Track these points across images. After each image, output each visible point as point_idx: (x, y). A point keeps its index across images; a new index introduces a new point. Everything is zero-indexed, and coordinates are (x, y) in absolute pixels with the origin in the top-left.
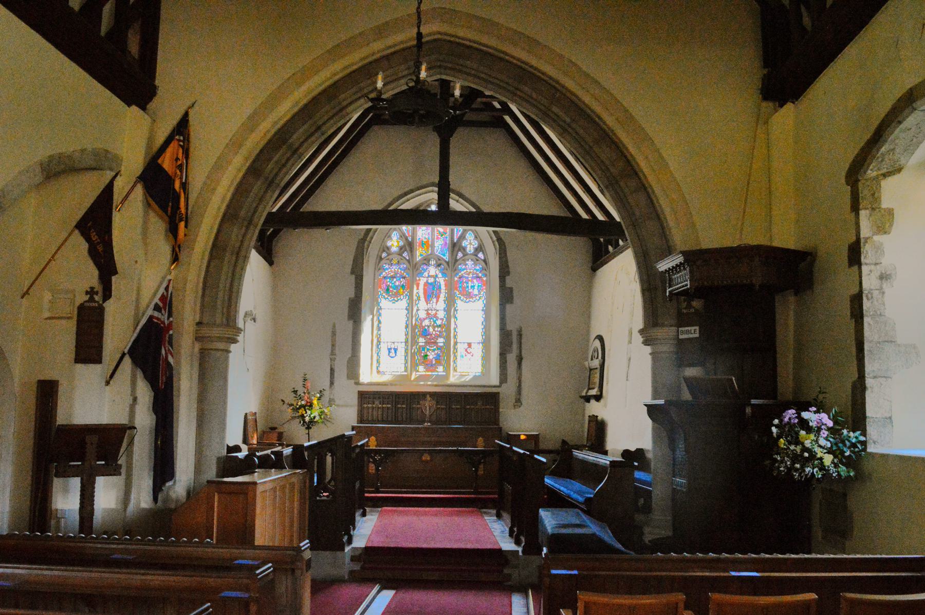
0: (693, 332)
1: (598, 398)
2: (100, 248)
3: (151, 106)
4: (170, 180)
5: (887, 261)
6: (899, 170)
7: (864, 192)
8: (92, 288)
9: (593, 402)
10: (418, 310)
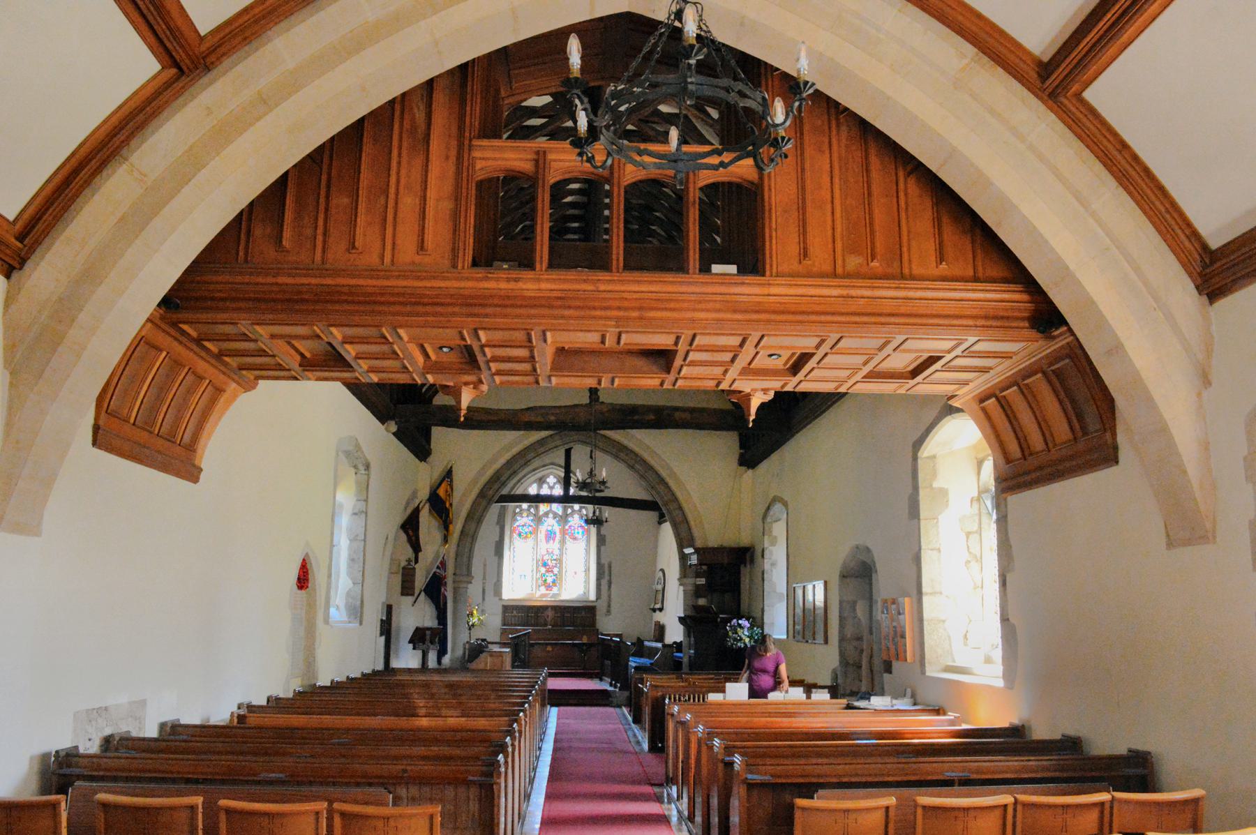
0: (702, 581)
1: (661, 610)
2: (413, 538)
3: (430, 459)
4: (443, 502)
9: (658, 612)
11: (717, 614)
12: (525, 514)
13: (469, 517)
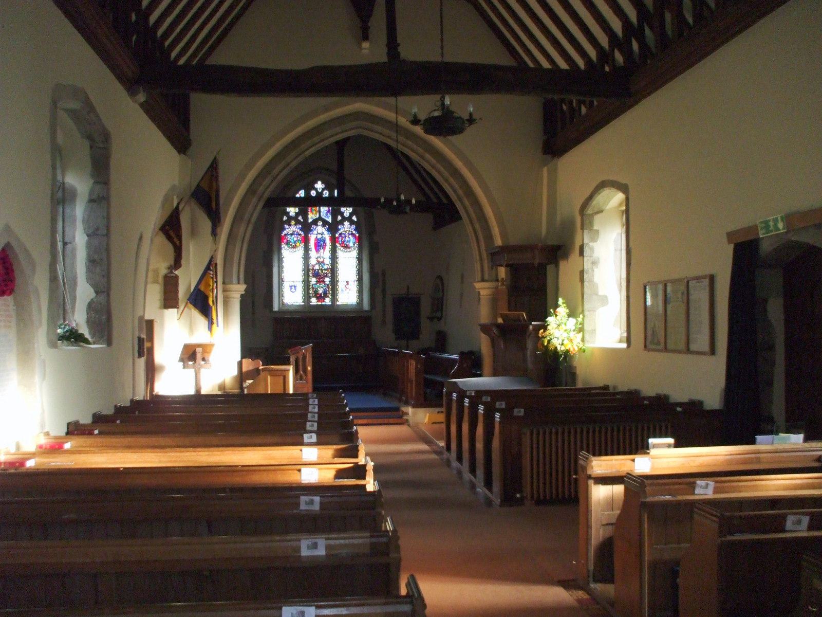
5: (596, 255)
7: (587, 221)
12: (293, 223)
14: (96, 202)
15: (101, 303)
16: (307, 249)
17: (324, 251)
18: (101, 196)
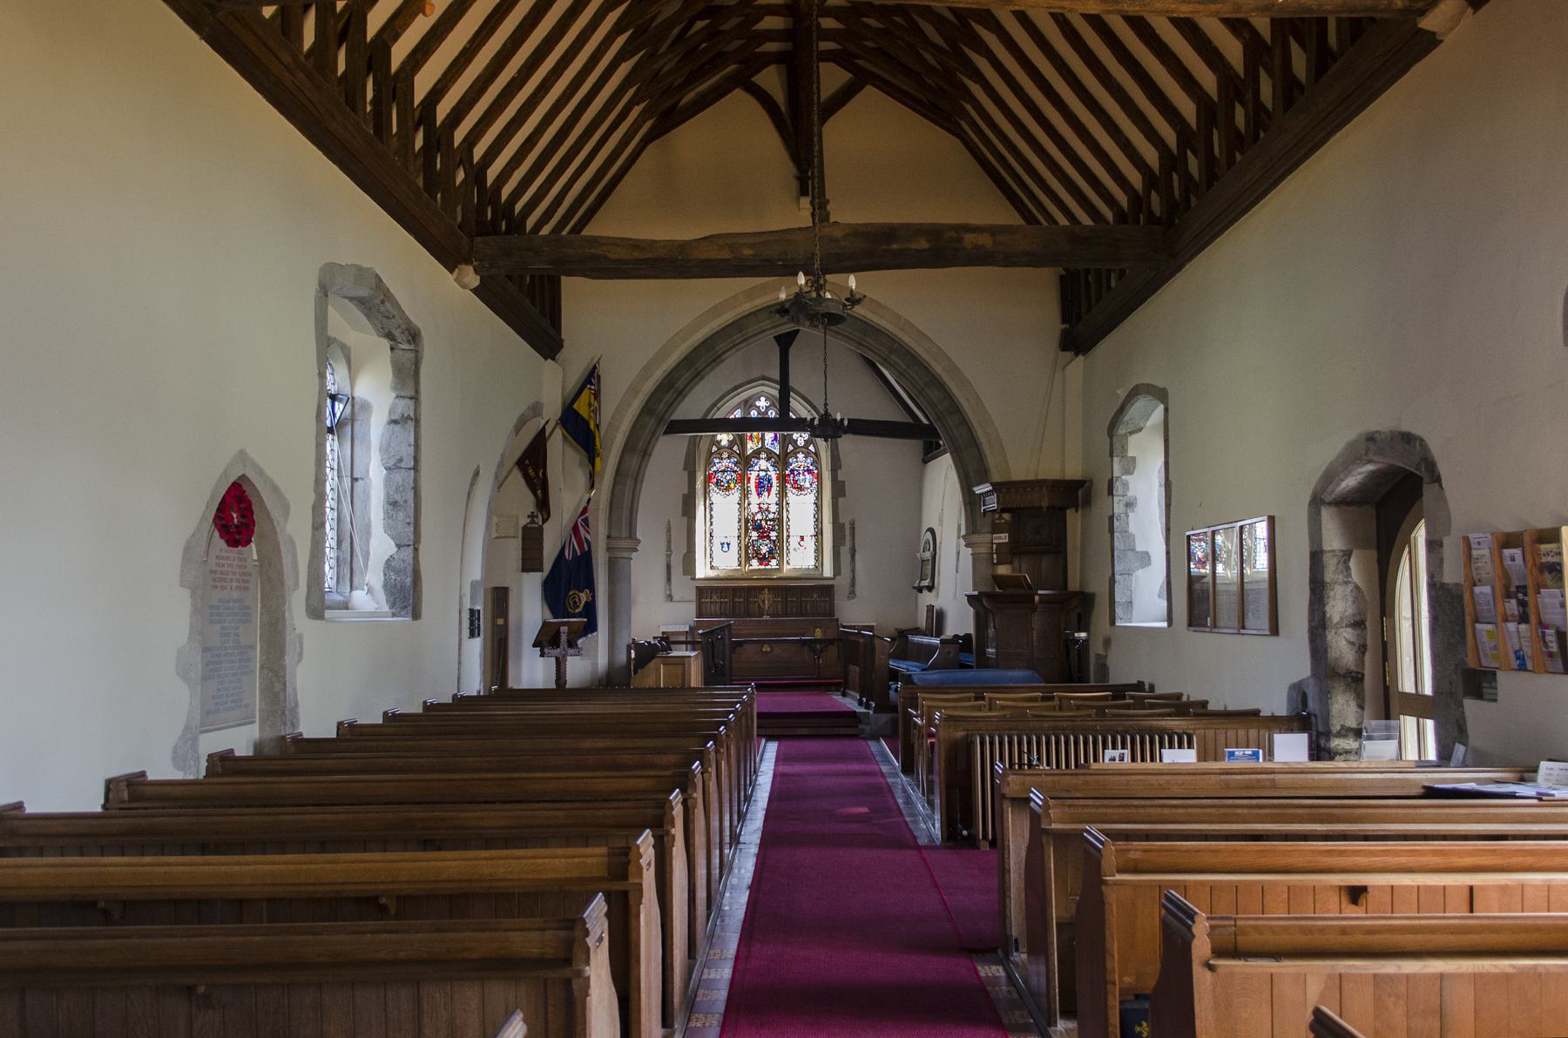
0: (1003, 538)
1: (930, 588)
3: (559, 356)
6: (1140, 430)
7: (1117, 445)
8: (533, 513)
9: (925, 592)
10: (749, 504)
11: (1032, 589)
13: (628, 448)
14: (399, 423)
15: (404, 561)
16: (745, 494)
17: (769, 495)
18: (406, 415)
